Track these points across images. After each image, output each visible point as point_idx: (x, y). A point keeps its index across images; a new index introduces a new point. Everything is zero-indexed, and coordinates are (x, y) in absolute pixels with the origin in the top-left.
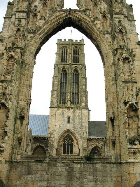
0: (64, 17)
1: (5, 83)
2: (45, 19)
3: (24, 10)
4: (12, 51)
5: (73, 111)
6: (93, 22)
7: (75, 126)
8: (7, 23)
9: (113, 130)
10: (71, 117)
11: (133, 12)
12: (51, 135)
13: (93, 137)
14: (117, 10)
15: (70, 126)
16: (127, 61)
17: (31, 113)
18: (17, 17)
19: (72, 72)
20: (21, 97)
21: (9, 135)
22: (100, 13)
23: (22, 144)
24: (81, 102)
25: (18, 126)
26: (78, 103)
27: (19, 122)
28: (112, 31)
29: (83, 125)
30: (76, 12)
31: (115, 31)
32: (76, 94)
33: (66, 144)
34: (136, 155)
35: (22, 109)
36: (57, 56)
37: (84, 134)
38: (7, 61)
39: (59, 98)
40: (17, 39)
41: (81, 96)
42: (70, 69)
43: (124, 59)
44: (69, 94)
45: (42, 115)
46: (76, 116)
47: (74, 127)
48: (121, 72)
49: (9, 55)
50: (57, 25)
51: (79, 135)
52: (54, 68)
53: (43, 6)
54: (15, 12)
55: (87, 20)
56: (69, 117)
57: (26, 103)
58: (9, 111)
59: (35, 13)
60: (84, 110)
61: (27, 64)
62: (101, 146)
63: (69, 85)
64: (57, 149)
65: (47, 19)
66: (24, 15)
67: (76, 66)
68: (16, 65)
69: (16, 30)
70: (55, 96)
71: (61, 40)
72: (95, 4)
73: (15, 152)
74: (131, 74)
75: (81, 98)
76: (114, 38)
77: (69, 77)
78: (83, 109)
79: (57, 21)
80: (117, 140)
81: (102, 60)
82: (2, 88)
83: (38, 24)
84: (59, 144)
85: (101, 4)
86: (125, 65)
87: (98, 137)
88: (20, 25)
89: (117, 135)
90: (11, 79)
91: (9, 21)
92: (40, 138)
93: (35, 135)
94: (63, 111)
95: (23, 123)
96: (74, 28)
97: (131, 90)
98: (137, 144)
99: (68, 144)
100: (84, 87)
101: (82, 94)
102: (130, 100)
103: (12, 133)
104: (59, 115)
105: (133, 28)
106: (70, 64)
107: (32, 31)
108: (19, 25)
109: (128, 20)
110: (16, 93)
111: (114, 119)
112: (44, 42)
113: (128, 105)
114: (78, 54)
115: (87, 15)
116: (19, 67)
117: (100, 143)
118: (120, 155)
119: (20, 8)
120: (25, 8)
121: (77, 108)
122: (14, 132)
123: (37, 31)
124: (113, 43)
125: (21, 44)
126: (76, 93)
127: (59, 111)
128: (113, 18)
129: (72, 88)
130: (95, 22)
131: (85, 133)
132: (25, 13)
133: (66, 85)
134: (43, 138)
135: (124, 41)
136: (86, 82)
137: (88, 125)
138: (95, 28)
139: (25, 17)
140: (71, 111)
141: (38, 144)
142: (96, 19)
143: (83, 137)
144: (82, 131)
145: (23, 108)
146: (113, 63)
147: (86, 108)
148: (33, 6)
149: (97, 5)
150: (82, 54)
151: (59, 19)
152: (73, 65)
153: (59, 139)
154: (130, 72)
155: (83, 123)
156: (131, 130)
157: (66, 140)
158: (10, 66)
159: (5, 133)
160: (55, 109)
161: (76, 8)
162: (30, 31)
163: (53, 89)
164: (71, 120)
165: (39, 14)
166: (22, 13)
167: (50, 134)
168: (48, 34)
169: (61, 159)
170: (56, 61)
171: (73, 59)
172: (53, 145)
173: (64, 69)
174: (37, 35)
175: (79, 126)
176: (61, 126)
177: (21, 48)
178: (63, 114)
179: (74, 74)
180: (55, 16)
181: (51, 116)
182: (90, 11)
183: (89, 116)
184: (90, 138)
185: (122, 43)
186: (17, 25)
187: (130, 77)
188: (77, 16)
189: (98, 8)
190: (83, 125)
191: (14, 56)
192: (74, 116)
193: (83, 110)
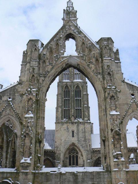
6: (88, 65)
8: (23, 69)
9: (105, 148)
10: (75, 131)
11: (119, 55)
15: (74, 140)
16: (113, 98)
18: (31, 65)
25: (38, 148)
27: (38, 145)
37: (88, 147)
39: (63, 114)
42: (72, 87)
43: (111, 97)
44: (73, 110)
47: (78, 141)
51: (83, 147)
52: (58, 86)
56: (74, 131)
58: (32, 139)
64: (63, 161)
65: (54, 64)
72: (90, 50)
74: (116, 108)
78: (85, 124)
80: (108, 155)
83: (47, 69)
84: (65, 157)
86: (112, 101)
88: (34, 72)
89: (107, 152)
92: (48, 151)
94: (68, 126)
99: (73, 156)
100: (86, 102)
101: (85, 109)
103: (34, 153)
104: (64, 130)
105: (119, 69)
108: (33, 73)
111: (105, 140)
113: (114, 131)
118: (110, 166)
120: (36, 56)
127: (64, 126)
129: (75, 105)
130: (90, 66)
134: (50, 151)
136: (88, 98)
144: (85, 143)
153: (65, 152)
155: (86, 137)
156: (116, 149)
159: (30, 154)
160: (60, 125)
161: (76, 54)
164: (75, 134)
165: (47, 60)
166: (35, 62)
168: (55, 76)
169: (13, 141)
172: (60, 157)
175: (83, 139)
176: (66, 140)
178: (68, 128)
179: (76, 91)
181: (57, 131)
189: (92, 53)
190: (87, 138)
192: (78, 130)
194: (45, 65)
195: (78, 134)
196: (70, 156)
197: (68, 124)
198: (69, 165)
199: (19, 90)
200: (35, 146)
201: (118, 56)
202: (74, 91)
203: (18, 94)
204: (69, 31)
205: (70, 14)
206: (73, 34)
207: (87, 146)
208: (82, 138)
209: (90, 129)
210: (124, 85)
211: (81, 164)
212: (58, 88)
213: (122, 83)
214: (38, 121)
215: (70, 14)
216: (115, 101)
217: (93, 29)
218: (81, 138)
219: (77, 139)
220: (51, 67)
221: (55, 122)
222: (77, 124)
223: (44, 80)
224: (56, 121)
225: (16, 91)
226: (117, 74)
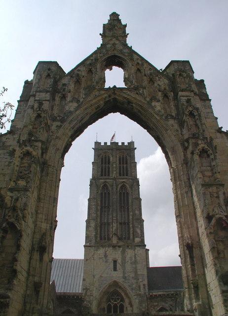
1: (16, 193)
2: (78, 101)
3: (48, 89)
6: (149, 103)
7: (126, 275)
10: (119, 261)
11: (205, 88)
12: (86, 292)
13: (155, 293)
14: (183, 87)
15: (117, 276)
17: (56, 255)
18: (37, 99)
19: (118, 190)
20: (40, 216)
21: (20, 276)
22: (159, 91)
23: (41, 293)
24: (133, 236)
26: (129, 238)
27: (36, 256)
28: (178, 114)
29: (139, 273)
31: (183, 113)
32: (125, 224)
35: (42, 236)
38: (19, 159)
39: (99, 231)
40: (36, 128)
41: (133, 227)
42: (115, 187)
44: (115, 225)
45: (73, 260)
46: (128, 258)
47: (124, 278)
48: (198, 171)
49: (23, 150)
50: (96, 109)
53: (75, 84)
55: (140, 101)
57: (48, 225)
61: (50, 165)
66: (48, 96)
67: (124, 182)
68: (34, 165)
69: (35, 115)
70: (91, 229)
71: (100, 143)
73: (27, 308)
74: (213, 173)
76: (181, 124)
77: (115, 198)
79: (96, 103)
81: (166, 158)
82: (12, 201)
83: (67, 108)
87: (165, 293)
90: (26, 186)
92: (69, 296)
93: (61, 293)
96: (122, 113)
97: (216, 197)
99: (115, 306)
100: (137, 212)
103: (25, 274)
105: (208, 110)
106: (115, 179)
108: (39, 110)
109: (201, 100)
110: (34, 209)
113: (213, 221)
114: (127, 164)
115: (141, 94)
116: (38, 168)
117: (167, 303)
119: (42, 87)
121: (128, 246)
122: (28, 273)
123: (66, 118)
124: (182, 131)
125: (43, 136)
127: (98, 252)
128: (179, 97)
130: (153, 104)
131: (142, 287)
132: (49, 93)
133: (108, 211)
134: (73, 297)
135: (199, 127)
138: (152, 112)
139: (48, 99)
142: (153, 98)
145: (44, 234)
146: (184, 160)
149: (153, 81)
151: (99, 101)
152: (120, 180)
154: (212, 170)
157: (112, 299)
158: (25, 166)
160: (92, 249)
162: (56, 118)
163: (88, 217)
164: (118, 266)
168: (83, 122)
170: (93, 174)
171: (118, 171)
173: (105, 186)
174: (66, 124)
177: (43, 142)
178: (106, 256)
179: (120, 193)
180: (92, 96)
182: (145, 88)
183: (147, 259)
184: (151, 294)
185: (194, 130)
186: (37, 109)
187: (212, 179)
189: (156, 85)
190: (139, 273)
191: (32, 152)
192: (124, 259)
193: (138, 248)
196: (109, 305)
198: (108, 312)
199: (8, 144)
200: (28, 257)
201: (204, 91)
206: (119, 57)
207: (139, 287)
210: (222, 137)
213: (218, 135)
214: (42, 205)
215: (114, 29)
216: (209, 159)
217: (157, 50)
219: (122, 275)
220: (75, 105)
223: (61, 126)
226: (206, 118)
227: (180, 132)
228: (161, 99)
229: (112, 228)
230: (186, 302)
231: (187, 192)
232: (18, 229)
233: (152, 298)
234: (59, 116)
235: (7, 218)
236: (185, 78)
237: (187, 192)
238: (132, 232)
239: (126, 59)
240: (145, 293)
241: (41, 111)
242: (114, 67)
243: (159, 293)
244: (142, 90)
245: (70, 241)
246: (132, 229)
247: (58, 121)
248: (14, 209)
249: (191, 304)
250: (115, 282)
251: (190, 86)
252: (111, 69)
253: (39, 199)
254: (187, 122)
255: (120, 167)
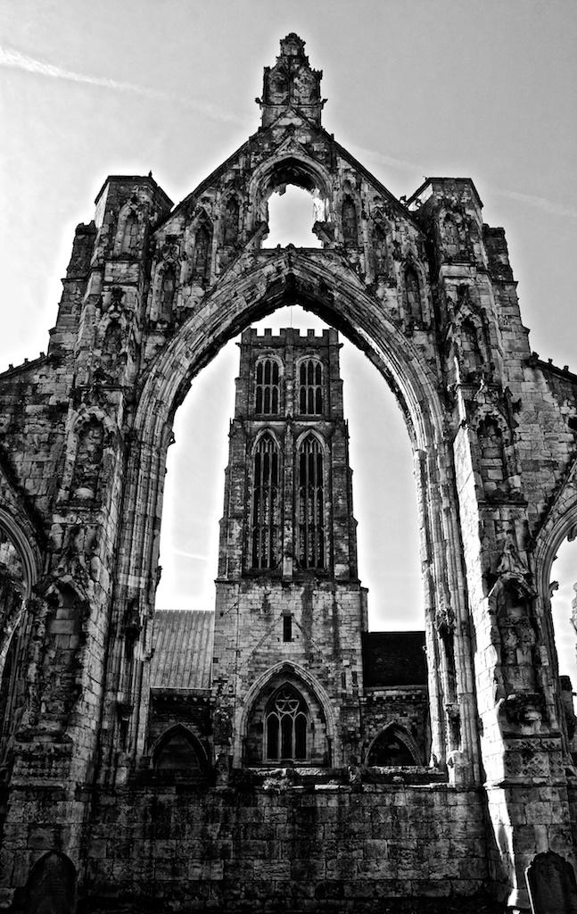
0: (269, 275)
4: (93, 402)
5: (302, 597)
6: (370, 291)
7: (313, 651)
8: (72, 298)
10: (298, 618)
12: (220, 687)
14: (450, 249)
15: (291, 651)
22: (396, 258)
27: (119, 647)
29: (343, 646)
30: (313, 258)
33: (280, 720)
34: (533, 759)
36: (240, 389)
37: (348, 682)
39: (250, 546)
41: (332, 538)
44: (288, 532)
47: (309, 656)
51: (326, 684)
54: (101, 261)
59: (171, 260)
60: (344, 589)
62: (413, 727)
63: (291, 505)
67: (311, 427)
69: (107, 323)
72: (378, 227)
75: (332, 543)
84: (253, 723)
85: (397, 229)
87: (402, 693)
91: (79, 292)
92: (181, 697)
94: (266, 595)
95: (135, 653)
96: (307, 308)
98: (533, 721)
99: (287, 720)
102: (506, 568)
103: (97, 688)
104: (253, 611)
107: (159, 325)
110: (110, 546)
112: (201, 362)
113: (498, 585)
115: (352, 267)
117: (406, 715)
122: (104, 684)
123: (177, 325)
124: (443, 364)
126: (312, 527)
127: (250, 597)
131: (349, 677)
137: (360, 648)
139: (135, 279)
140: (297, 595)
141: (172, 723)
142: (382, 275)
143: (345, 691)
145: (136, 601)
147: (352, 579)
148: (160, 236)
150: (333, 381)
152: (301, 423)
153: (255, 703)
154: (504, 467)
157: (281, 705)
163: (226, 513)
164: (294, 628)
165: (183, 264)
167: (217, 684)
168: (217, 333)
171: (298, 400)
172: (229, 724)
175: (328, 650)
176: (258, 654)
178: (266, 605)
179: (303, 456)
188: (318, 270)
192: (308, 612)
194: (171, 284)
195: (310, 629)
197: (268, 588)
199: (45, 390)
201: (502, 258)
202: (295, 454)
203: (40, 407)
204: (296, 131)
205: (291, 75)
208: (324, 644)
209: (354, 611)
210: (536, 378)
211: (318, 751)
212: (230, 442)
215: (291, 75)
218: (321, 647)
221: (215, 576)
222: (303, 589)
224: (220, 573)
225: (29, 392)
227: (439, 367)
228: (399, 279)
229: (282, 539)
230: (436, 748)
231: (447, 511)
232: (79, 598)
233: (371, 704)
234: (162, 322)
235: (56, 573)
236: (458, 225)
237: (447, 511)
238: (328, 550)
239: (319, 169)
240: (355, 693)
241: (119, 312)
242: (290, 187)
243: (389, 693)
244: (355, 256)
245: (188, 573)
246: (328, 543)
247: (160, 334)
248: (71, 553)
249: (443, 753)
250: (287, 666)
251: (469, 246)
252: (283, 191)
253: (121, 524)
254: (456, 344)
255: (303, 391)
